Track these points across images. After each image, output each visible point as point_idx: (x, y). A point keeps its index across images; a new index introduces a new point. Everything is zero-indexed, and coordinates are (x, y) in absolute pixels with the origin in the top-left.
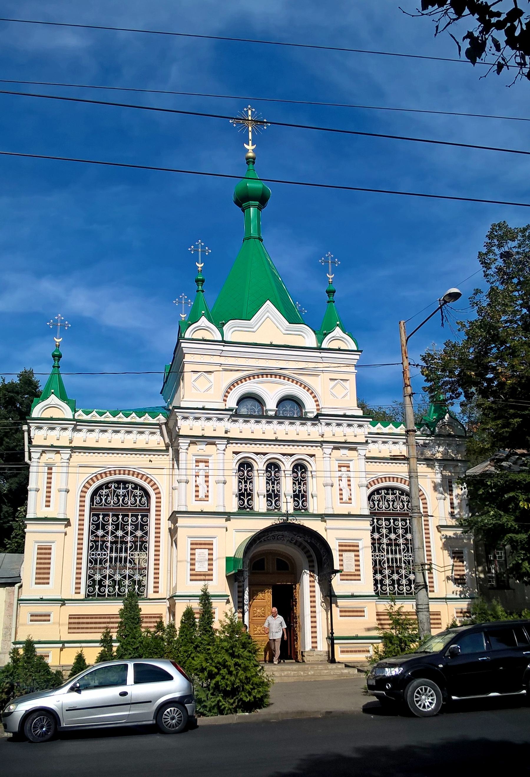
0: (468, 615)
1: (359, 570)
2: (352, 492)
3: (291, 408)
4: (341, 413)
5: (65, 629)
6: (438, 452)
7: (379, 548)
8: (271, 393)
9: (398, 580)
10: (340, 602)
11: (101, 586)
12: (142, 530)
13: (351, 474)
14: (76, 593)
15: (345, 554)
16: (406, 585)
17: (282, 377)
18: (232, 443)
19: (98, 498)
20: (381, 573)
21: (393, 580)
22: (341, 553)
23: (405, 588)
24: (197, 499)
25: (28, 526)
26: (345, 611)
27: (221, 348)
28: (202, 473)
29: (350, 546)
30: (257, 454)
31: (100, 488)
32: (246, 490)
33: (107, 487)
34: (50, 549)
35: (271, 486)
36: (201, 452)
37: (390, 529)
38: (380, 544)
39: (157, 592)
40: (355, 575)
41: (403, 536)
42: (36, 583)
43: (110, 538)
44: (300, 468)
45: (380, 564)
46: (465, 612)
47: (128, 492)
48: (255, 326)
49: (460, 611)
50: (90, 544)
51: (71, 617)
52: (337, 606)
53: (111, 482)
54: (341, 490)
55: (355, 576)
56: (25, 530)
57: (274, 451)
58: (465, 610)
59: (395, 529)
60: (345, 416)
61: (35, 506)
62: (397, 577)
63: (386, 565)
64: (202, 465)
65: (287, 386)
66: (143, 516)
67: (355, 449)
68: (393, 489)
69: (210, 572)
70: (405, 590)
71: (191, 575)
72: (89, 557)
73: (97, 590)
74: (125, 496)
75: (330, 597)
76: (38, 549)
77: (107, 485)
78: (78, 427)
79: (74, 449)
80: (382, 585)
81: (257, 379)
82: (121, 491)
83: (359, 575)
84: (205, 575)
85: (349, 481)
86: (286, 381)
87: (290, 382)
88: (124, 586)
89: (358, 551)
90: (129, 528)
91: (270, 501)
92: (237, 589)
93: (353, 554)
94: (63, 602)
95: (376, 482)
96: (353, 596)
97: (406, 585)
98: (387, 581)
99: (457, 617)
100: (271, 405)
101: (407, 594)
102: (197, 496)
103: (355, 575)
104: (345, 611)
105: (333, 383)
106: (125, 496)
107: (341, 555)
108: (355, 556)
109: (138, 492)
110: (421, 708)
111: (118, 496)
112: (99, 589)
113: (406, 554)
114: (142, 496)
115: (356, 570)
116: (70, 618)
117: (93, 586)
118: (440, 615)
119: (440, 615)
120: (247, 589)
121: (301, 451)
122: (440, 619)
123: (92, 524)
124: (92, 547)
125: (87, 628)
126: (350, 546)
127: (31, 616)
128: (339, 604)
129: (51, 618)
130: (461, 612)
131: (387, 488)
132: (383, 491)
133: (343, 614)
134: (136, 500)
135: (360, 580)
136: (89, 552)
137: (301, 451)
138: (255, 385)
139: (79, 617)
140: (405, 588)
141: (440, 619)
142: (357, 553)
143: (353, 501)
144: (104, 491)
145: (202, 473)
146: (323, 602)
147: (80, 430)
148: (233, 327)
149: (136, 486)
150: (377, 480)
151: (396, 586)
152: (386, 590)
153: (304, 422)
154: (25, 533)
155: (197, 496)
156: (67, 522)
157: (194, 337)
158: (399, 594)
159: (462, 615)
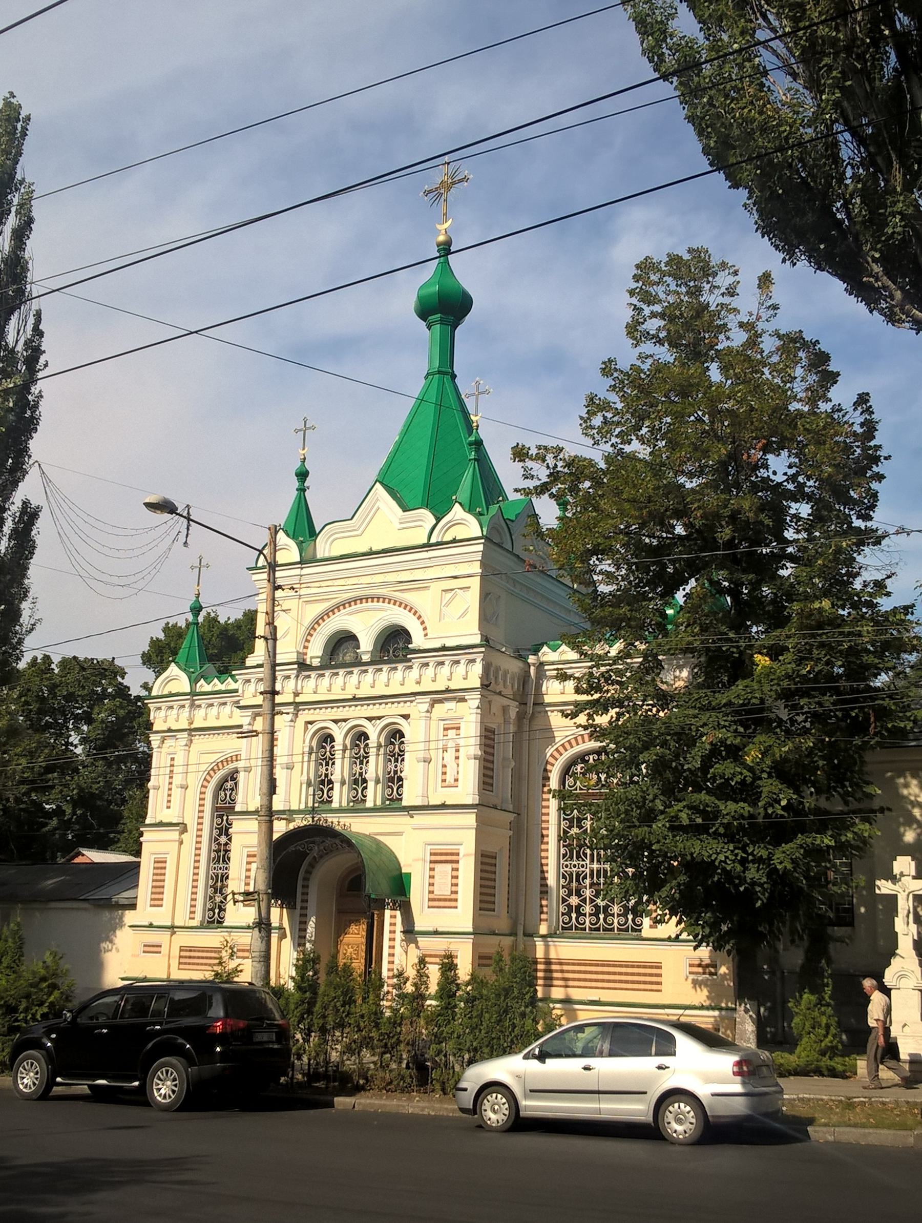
0: (713, 970)
1: (456, 892)
3: (394, 644)
4: (437, 645)
5: (175, 963)
6: (679, 678)
8: (366, 627)
9: (578, 907)
10: (421, 940)
11: (579, 914)
13: (462, 742)
14: (190, 918)
15: (438, 867)
16: (619, 915)
17: (358, 602)
18: (304, 710)
19: (223, 794)
20: (579, 894)
21: (570, 906)
22: (433, 865)
23: (616, 921)
24: (444, 784)
25: (145, 834)
26: (149, 946)
27: (298, 572)
28: (451, 744)
29: (447, 854)
34: (165, 862)
35: (393, 765)
36: (451, 714)
40: (450, 900)
42: (151, 906)
44: (396, 735)
45: (578, 880)
46: (707, 966)
48: (359, 527)
49: (697, 962)
50: (562, 851)
51: (182, 949)
52: (417, 947)
53: (589, 753)
54: (444, 766)
55: (450, 901)
56: (141, 839)
57: (357, 713)
58: (707, 961)
60: (444, 648)
61: (156, 810)
62: (571, 900)
63: (588, 881)
64: (452, 733)
65: (389, 612)
67: (463, 700)
69: (453, 896)
70: (616, 924)
71: (430, 900)
72: (562, 870)
73: (630, 921)
76: (155, 862)
78: (197, 702)
79: (192, 731)
80: (579, 914)
81: (348, 609)
83: (456, 900)
84: (445, 900)
85: (457, 751)
86: (386, 604)
87: (391, 605)
88: (613, 915)
89: (457, 862)
91: (355, 789)
92: (298, 919)
93: (449, 867)
94: (172, 928)
95: (573, 742)
96: (436, 933)
97: (619, 915)
98: (588, 909)
99: (690, 973)
100: (366, 644)
101: (590, 929)
102: (444, 781)
103: (450, 900)
105: (449, 596)
107: (432, 869)
108: (453, 869)
110: (154, 1087)
112: (605, 920)
113: (567, 863)
115: (452, 892)
116: (181, 950)
117: (569, 914)
118: (660, 968)
119: (660, 968)
120: (313, 919)
121: (390, 711)
122: (660, 975)
123: (564, 819)
125: (198, 964)
126: (447, 854)
127: (145, 946)
128: (420, 944)
129: (162, 949)
130: (699, 965)
132: (591, 757)
135: (456, 907)
136: (562, 862)
138: (347, 617)
139: (191, 949)
140: (616, 921)
141: (660, 975)
142: (455, 866)
143: (460, 783)
144: (579, 768)
145: (451, 744)
146: (403, 940)
147: (200, 706)
148: (332, 535)
150: (576, 738)
151: (574, 915)
152: (612, 924)
153: (393, 666)
154: (141, 843)
155: (444, 781)
156: (183, 828)
158: (605, 930)
159: (700, 970)
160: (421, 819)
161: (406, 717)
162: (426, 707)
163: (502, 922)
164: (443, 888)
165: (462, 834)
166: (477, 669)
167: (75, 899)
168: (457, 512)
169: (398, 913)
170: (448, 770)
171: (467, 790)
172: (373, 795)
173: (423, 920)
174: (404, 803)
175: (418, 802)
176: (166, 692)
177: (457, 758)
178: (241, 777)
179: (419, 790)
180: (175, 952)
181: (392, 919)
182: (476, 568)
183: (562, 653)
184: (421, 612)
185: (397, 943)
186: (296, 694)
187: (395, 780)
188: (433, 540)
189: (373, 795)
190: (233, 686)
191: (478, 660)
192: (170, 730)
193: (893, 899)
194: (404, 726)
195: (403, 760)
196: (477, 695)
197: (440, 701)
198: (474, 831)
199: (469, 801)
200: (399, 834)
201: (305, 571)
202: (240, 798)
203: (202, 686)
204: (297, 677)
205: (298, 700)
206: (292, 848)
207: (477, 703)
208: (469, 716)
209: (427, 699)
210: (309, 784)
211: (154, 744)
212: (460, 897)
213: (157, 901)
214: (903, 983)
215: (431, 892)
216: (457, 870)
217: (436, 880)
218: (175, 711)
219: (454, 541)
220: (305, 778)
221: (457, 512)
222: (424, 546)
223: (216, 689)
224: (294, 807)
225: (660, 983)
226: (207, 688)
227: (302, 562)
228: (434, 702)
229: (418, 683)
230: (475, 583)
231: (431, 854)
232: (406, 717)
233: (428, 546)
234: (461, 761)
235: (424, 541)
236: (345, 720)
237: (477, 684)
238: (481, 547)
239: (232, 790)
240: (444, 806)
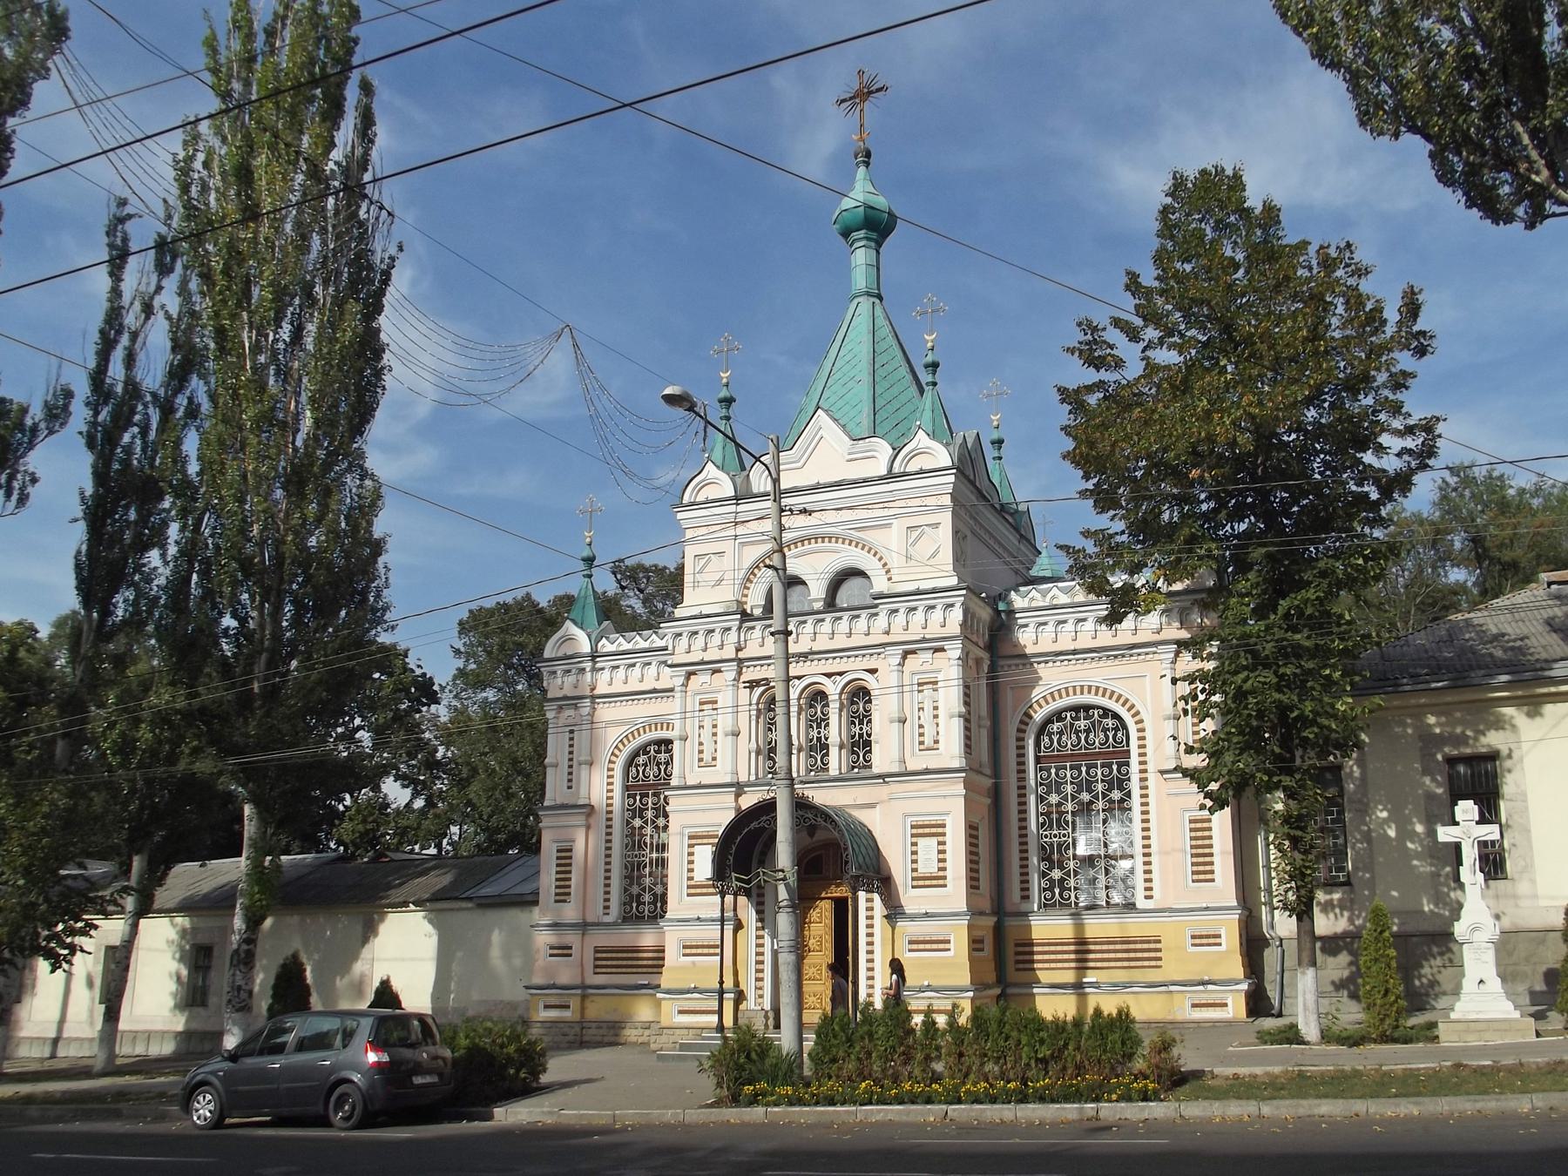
1: (944, 869)
2: (941, 729)
4: (911, 587)
7: (1058, 820)
12: (1121, 788)
15: (921, 841)
20: (1061, 868)
21: (1051, 880)
26: (1201, 937)
27: (733, 508)
30: (829, 675)
31: (636, 754)
32: (861, 736)
33: (1060, 719)
36: (926, 667)
37: (1079, 785)
38: (1061, 813)
39: (1151, 897)
41: (1104, 795)
43: (1069, 807)
44: (859, 695)
45: (1059, 851)
47: (1093, 724)
53: (649, 744)
54: (921, 726)
55: (937, 880)
59: (1058, 784)
66: (1120, 765)
67: (942, 650)
68: (1087, 708)
74: (1088, 731)
75: (894, 912)
77: (643, 749)
82: (1082, 724)
83: (945, 878)
86: (840, 545)
90: (1100, 787)
93: (934, 840)
102: (921, 743)
104: (1201, 937)
105: (915, 534)
106: (1088, 731)
109: (1110, 722)
111: (1077, 732)
114: (1116, 729)
115: (940, 869)
117: (1051, 889)
124: (1043, 825)
127: (1193, 937)
129: (573, 951)
131: (1076, 709)
133: (1198, 941)
134: (1107, 737)
137: (854, 667)
143: (941, 745)
144: (1056, 727)
147: (1026, 626)
149: (1106, 712)
151: (1057, 891)
157: (700, 498)
160: (895, 788)
161: (873, 671)
162: (897, 660)
163: (986, 905)
164: (928, 865)
165: (949, 805)
166: (957, 615)
167: (456, 899)
168: (922, 439)
169: (876, 896)
170: (926, 730)
171: (951, 751)
172: (836, 761)
173: (912, 899)
174: (876, 770)
175: (895, 769)
176: (560, 654)
177: (936, 717)
178: (676, 746)
179: (895, 755)
180: (589, 956)
181: (869, 906)
182: (947, 500)
183: (1032, 599)
184: (883, 552)
185: (877, 930)
186: (738, 650)
187: (860, 745)
188: (896, 470)
189: (836, 761)
190: (659, 643)
191: (958, 605)
192: (565, 698)
193: (1457, 847)
194: (871, 682)
195: (827, 725)
196: (958, 644)
197: (914, 652)
198: (962, 800)
199: (956, 764)
200: (872, 806)
201: (740, 508)
202: (676, 771)
203: (1053, 597)
204: (739, 628)
205: (741, 655)
206: (754, 825)
207: (958, 653)
208: (949, 668)
209: (899, 650)
210: (758, 753)
211: (550, 715)
212: (949, 873)
213: (562, 896)
214: (1477, 936)
215: (914, 870)
216: (944, 843)
217: (920, 857)
218: (637, 669)
219: (922, 472)
220: (753, 745)
221: (922, 439)
222: (881, 478)
223: (1034, 604)
224: (743, 778)
225: (1160, 959)
226: (610, 648)
227: (738, 498)
228: (906, 654)
229: (887, 633)
230: (946, 519)
231: (913, 827)
232: (873, 671)
233: (891, 476)
234: (940, 720)
235: (884, 472)
236: (841, 674)
237: (957, 630)
238: (952, 479)
239: (667, 764)
240: (927, 772)
